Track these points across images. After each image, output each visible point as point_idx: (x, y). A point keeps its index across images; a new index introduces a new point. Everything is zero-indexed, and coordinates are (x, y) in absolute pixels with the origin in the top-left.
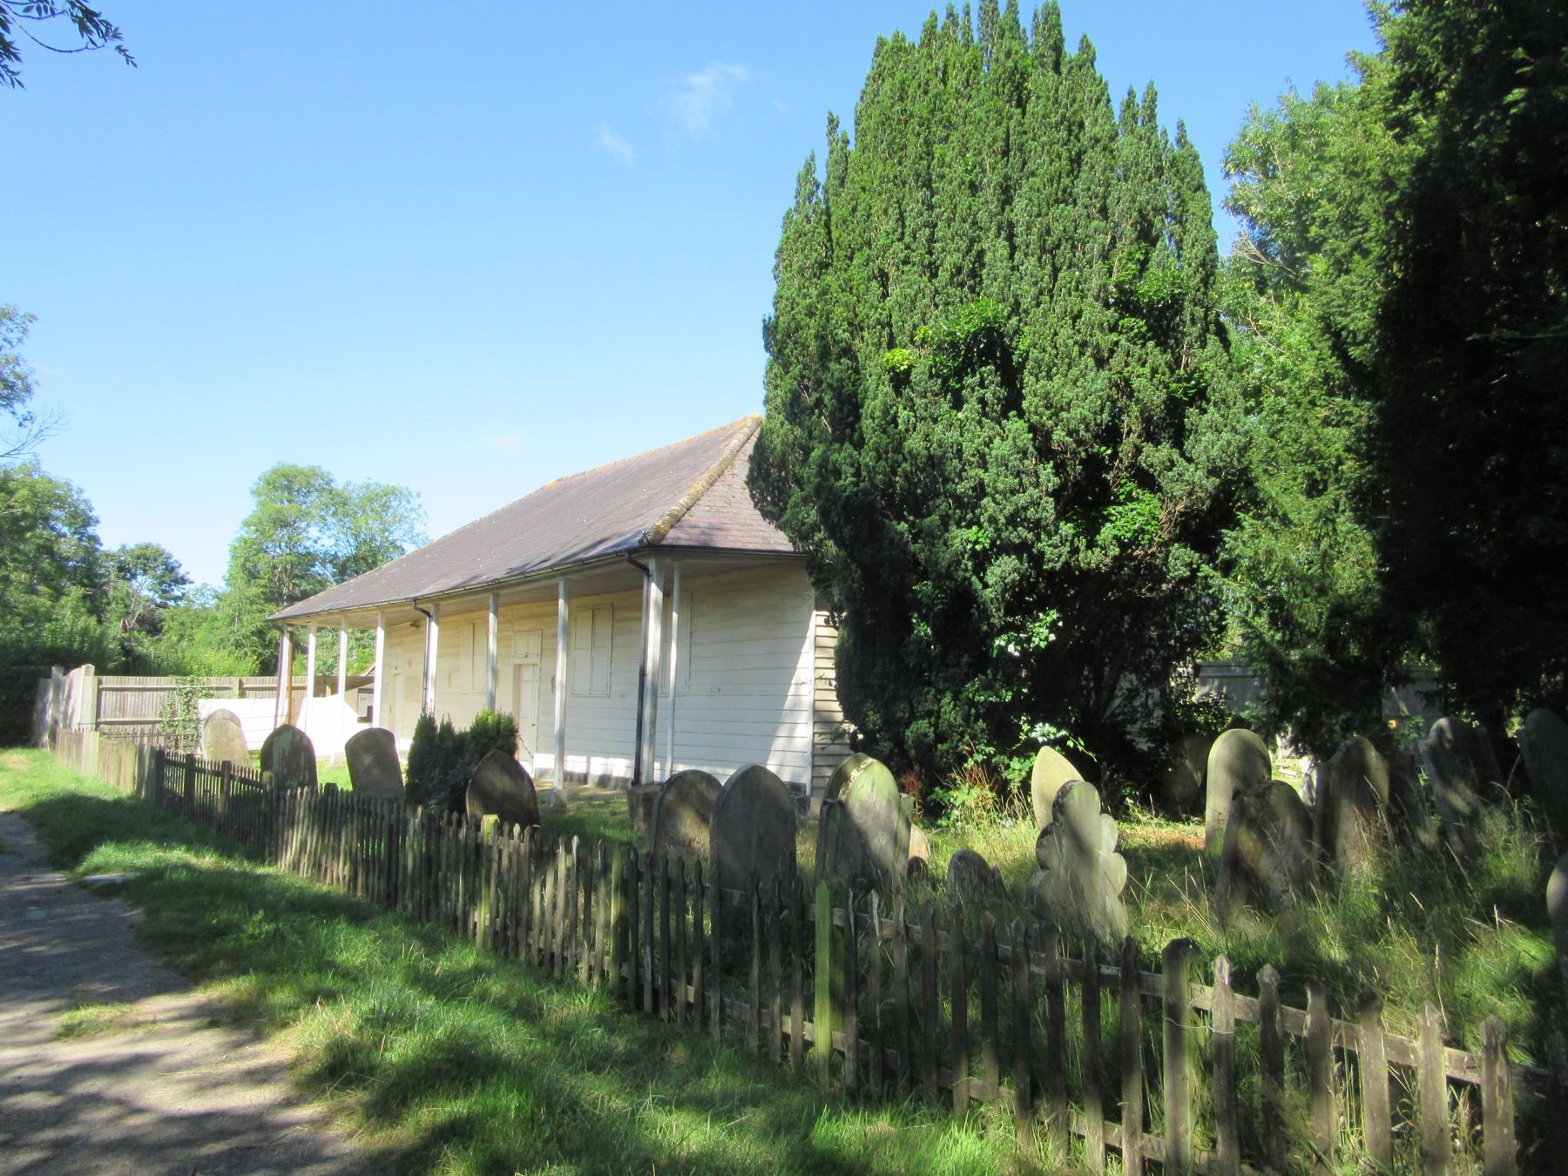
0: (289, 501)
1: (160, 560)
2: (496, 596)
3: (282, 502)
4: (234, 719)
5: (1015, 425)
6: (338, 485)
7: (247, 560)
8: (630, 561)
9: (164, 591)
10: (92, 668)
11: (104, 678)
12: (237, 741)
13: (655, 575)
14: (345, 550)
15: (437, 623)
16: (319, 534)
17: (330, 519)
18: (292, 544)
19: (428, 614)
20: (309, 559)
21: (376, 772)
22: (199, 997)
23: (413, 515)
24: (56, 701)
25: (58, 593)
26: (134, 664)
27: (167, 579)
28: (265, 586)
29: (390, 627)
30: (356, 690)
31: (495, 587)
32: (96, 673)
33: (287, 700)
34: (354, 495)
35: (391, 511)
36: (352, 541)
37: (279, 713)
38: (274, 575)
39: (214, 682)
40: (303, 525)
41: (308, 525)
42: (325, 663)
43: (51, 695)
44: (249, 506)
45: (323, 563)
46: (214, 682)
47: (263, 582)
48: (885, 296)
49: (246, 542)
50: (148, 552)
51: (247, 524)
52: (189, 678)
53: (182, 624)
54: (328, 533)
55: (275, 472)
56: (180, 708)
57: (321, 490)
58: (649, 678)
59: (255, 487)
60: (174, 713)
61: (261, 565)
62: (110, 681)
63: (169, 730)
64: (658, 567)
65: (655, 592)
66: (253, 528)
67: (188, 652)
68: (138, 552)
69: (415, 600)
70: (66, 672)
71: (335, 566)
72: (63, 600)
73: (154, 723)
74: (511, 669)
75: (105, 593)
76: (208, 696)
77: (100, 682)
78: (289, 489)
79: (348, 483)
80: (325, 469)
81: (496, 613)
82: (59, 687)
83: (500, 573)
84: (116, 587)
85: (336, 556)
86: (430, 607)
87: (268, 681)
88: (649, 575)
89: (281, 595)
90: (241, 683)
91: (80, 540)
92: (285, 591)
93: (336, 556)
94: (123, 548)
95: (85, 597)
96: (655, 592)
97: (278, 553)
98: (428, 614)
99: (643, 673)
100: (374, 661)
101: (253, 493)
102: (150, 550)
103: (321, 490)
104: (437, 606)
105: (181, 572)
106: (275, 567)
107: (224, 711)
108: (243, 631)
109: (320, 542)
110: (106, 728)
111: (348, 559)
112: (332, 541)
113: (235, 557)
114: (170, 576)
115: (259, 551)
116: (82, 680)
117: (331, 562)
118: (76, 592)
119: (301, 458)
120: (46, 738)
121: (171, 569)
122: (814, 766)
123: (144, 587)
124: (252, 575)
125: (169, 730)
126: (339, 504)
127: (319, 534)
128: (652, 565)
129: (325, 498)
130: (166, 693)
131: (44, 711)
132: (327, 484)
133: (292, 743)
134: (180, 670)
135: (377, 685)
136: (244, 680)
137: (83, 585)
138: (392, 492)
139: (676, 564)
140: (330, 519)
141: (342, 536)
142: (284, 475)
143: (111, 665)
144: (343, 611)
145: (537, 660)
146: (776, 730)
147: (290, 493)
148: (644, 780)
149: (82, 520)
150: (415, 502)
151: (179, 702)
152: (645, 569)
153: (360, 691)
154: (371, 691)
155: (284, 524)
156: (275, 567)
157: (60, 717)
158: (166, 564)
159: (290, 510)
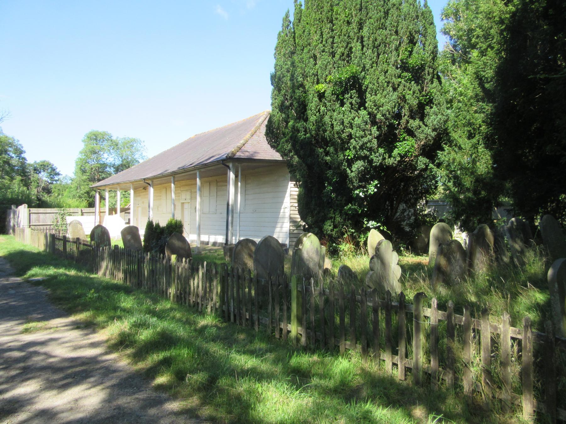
0: (96, 144)
1: (50, 166)
2: (174, 177)
3: (93, 144)
4: (80, 223)
5: (363, 112)
6: (114, 138)
7: (82, 166)
8: (223, 164)
9: (52, 178)
10: (26, 205)
11: (31, 209)
12: (81, 231)
13: (232, 169)
14: (118, 162)
15: (153, 188)
16: (108, 157)
17: (112, 151)
18: (98, 161)
19: (149, 184)
20: (104, 166)
21: (132, 241)
22: (72, 318)
23: (142, 149)
24: (14, 218)
25: (12, 179)
26: (42, 204)
27: (52, 173)
28: (89, 176)
29: (135, 189)
30: (124, 213)
31: (174, 174)
32: (28, 207)
33: (99, 217)
34: (120, 142)
35: (134, 148)
36: (120, 159)
37: (96, 221)
38: (92, 172)
39: (72, 210)
40: (102, 153)
41: (104, 153)
42: (112, 203)
43: (12, 215)
44: (82, 146)
45: (110, 167)
46: (72, 210)
47: (88, 174)
48: (315, 64)
49: (81, 159)
50: (45, 164)
51: (81, 153)
52: (62, 209)
53: (59, 190)
54: (111, 156)
55: (90, 133)
56: (60, 220)
57: (108, 140)
58: (230, 207)
59: (83, 139)
60: (57, 222)
61: (87, 168)
62: (33, 210)
63: (56, 228)
64: (233, 166)
65: (232, 175)
66: (83, 154)
67: (61, 199)
68: (41, 164)
69: (144, 179)
70: (17, 207)
71: (114, 168)
72: (14, 181)
73: (51, 225)
74: (180, 204)
75: (30, 179)
76: (69, 215)
77: (30, 211)
78: (96, 139)
79: (118, 137)
80: (109, 132)
81: (174, 184)
82: (15, 213)
83: (175, 169)
84: (34, 177)
85: (114, 165)
86: (150, 182)
87: (91, 210)
88: (230, 169)
89: (95, 179)
90: (82, 211)
91: (19, 159)
92: (96, 177)
93: (114, 165)
94: (35, 162)
95: (22, 180)
96: (232, 175)
97: (93, 163)
98: (149, 184)
99: (228, 205)
100: (130, 202)
101: (83, 141)
102: (46, 163)
103: (108, 140)
104: (152, 181)
105: (58, 171)
106: (92, 169)
107: (76, 220)
108: (81, 192)
109: (108, 160)
110: (33, 227)
111: (119, 166)
112: (113, 159)
113: (77, 165)
114: (53, 172)
115: (86, 163)
116: (23, 210)
117: (113, 167)
118: (19, 178)
119: (100, 128)
120: (11, 231)
121: (53, 170)
122: (290, 238)
123: (44, 176)
124: (84, 172)
125: (56, 228)
126: (115, 145)
127: (108, 157)
128: (231, 165)
129: (110, 143)
130: (54, 214)
131: (10, 222)
132: (110, 138)
133: (101, 231)
134: (59, 206)
135: (131, 211)
136: (83, 209)
137: (22, 176)
138: (134, 141)
139: (239, 165)
140: (112, 151)
141: (116, 157)
142: (94, 135)
143: (33, 204)
144: (118, 184)
145: (189, 201)
146: (276, 225)
147: (96, 141)
148: (229, 243)
149: (19, 152)
150: (143, 144)
151: (59, 217)
152: (228, 167)
153: (125, 213)
154: (129, 213)
155: (95, 153)
156: (92, 169)
157: (16, 224)
158: (52, 168)
159: (97, 148)
